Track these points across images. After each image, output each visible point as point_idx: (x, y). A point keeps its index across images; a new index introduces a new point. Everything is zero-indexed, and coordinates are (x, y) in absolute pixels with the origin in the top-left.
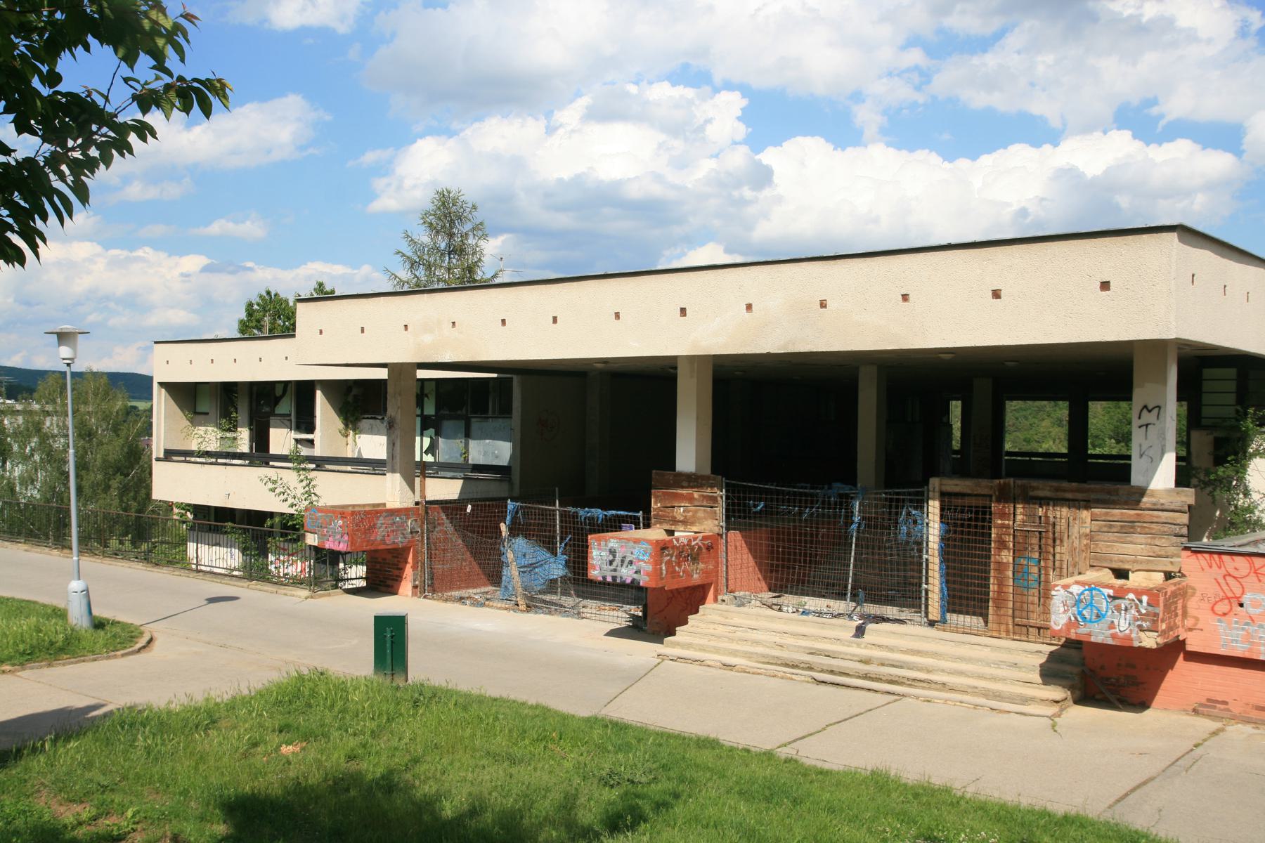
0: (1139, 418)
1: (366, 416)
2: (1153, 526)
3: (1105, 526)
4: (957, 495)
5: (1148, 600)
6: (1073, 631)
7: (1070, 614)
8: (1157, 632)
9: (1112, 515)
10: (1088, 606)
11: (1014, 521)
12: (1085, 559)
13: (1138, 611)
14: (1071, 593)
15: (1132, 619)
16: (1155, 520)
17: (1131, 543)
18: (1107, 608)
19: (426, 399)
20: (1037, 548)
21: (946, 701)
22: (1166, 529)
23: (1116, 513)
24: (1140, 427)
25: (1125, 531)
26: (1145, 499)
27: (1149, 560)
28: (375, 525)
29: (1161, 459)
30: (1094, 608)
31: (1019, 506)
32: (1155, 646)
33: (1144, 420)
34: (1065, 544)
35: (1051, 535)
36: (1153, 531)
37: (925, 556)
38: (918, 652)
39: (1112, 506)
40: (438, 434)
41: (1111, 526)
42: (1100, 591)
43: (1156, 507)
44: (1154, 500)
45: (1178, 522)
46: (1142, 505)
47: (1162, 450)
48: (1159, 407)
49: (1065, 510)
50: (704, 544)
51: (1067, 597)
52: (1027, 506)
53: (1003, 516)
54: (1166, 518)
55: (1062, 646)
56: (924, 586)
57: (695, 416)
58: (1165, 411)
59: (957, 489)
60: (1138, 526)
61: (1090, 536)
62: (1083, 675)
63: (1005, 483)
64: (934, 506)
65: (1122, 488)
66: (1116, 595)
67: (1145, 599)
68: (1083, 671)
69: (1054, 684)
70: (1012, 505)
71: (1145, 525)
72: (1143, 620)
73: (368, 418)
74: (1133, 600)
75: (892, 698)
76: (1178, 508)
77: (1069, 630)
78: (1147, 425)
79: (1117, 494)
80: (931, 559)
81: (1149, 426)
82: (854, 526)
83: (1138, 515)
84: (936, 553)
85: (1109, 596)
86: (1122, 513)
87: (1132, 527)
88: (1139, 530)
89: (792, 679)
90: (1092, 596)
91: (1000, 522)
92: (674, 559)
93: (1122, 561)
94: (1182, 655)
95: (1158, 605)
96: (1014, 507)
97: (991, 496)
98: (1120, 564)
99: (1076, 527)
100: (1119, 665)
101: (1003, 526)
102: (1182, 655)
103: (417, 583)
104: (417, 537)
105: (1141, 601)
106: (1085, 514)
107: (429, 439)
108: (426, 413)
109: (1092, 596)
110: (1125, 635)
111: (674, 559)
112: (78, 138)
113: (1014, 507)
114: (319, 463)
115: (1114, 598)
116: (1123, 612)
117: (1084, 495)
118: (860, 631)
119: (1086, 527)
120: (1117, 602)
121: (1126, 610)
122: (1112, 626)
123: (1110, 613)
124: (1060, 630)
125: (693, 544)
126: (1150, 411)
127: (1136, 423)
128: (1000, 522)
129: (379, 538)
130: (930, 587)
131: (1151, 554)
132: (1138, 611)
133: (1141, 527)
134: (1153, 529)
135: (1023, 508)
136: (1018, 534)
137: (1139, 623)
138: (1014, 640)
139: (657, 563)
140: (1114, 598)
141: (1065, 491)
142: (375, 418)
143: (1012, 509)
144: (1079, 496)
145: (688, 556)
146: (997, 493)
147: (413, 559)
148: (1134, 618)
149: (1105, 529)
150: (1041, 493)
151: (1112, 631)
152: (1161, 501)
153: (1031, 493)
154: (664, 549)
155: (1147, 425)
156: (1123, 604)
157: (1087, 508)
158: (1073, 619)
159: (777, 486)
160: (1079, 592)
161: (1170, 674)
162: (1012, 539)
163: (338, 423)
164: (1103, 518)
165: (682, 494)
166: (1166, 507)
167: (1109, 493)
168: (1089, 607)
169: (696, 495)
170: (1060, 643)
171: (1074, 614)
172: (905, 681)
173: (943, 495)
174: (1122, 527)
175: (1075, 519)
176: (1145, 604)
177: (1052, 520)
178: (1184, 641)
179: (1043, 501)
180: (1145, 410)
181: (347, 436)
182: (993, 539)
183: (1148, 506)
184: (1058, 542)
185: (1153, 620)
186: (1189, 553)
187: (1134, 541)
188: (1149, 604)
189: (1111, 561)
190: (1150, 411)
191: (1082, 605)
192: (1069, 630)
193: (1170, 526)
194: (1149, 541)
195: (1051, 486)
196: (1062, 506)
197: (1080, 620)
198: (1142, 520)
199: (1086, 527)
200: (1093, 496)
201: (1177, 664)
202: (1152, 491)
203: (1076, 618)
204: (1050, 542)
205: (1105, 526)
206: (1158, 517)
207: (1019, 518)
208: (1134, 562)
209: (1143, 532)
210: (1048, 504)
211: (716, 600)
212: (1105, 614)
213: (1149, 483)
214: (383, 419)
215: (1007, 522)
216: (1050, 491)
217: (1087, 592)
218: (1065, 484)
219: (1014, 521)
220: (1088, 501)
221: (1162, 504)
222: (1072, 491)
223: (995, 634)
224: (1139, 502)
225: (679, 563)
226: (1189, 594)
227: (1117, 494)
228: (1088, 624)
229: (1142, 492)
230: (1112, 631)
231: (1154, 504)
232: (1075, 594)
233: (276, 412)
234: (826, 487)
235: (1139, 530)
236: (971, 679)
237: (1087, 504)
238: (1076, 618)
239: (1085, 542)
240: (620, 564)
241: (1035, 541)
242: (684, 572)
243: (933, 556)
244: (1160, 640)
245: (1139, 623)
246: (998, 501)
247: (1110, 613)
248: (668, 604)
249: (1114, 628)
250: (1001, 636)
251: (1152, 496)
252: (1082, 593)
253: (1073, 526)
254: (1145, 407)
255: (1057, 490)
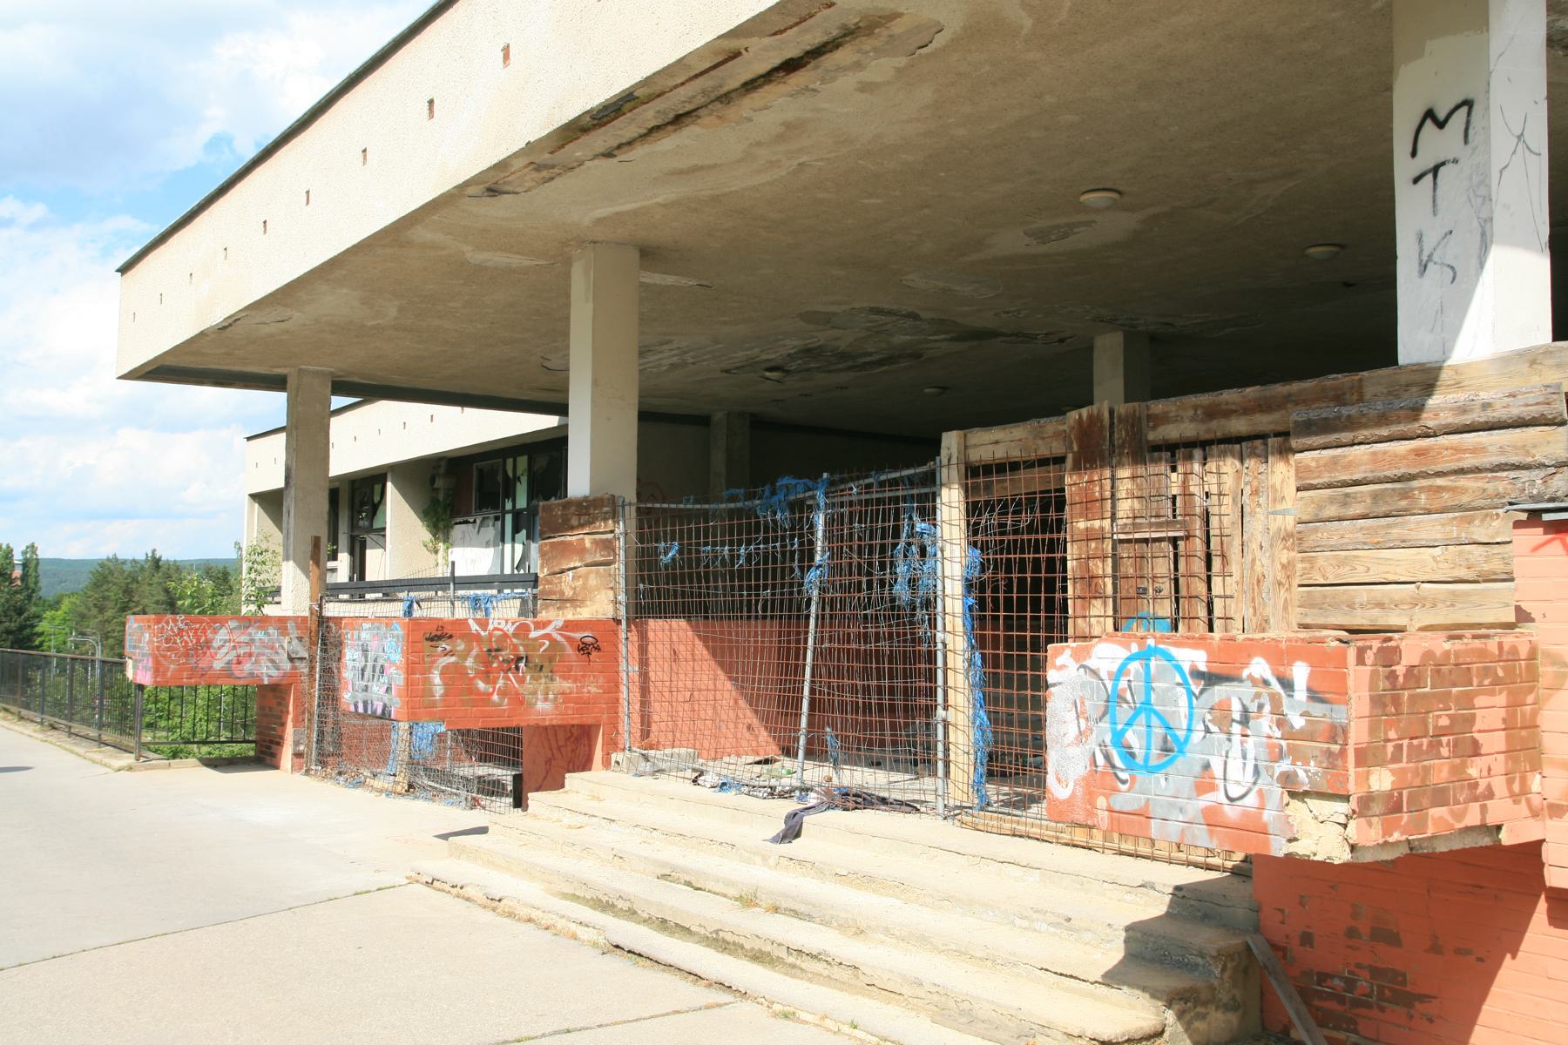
0: (1414, 154)
1: (458, 520)
2: (1462, 481)
3: (1332, 500)
4: (1001, 468)
5: (1312, 676)
6: (1101, 802)
7: (1092, 744)
8: (1346, 798)
9: (1349, 466)
10: (1137, 712)
11: (1113, 518)
12: (1285, 608)
13: (1282, 723)
14: (1095, 673)
15: (1263, 755)
16: (1469, 461)
17: (1405, 545)
18: (1191, 717)
19: (518, 484)
20: (1167, 587)
21: (825, 1017)
22: (1501, 487)
23: (1359, 457)
24: (1416, 180)
25: (1383, 509)
26: (1434, 401)
27: (1453, 593)
28: (208, 643)
29: (1482, 265)
30: (1154, 721)
31: (1124, 473)
32: (1342, 856)
33: (1425, 160)
34: (1234, 568)
35: (1198, 545)
36: (1465, 499)
37: (940, 636)
38: (866, 880)
39: (1346, 436)
40: (530, 537)
41: (1346, 501)
42: (1170, 658)
43: (1467, 419)
44: (1461, 397)
45: (1539, 458)
46: (1428, 420)
47: (1483, 234)
48: (1468, 103)
49: (1230, 465)
50: (569, 639)
51: (1083, 685)
52: (1140, 470)
53: (1089, 506)
54: (1502, 450)
55: (1236, 872)
56: (940, 712)
57: (589, 382)
58: (1487, 108)
59: (1000, 453)
60: (1421, 489)
61: (1295, 539)
62: (1244, 964)
63: (1090, 416)
64: (951, 502)
65: (1374, 380)
66: (1217, 668)
67: (1300, 673)
68: (1248, 948)
69: (1132, 985)
70: (1107, 473)
71: (1440, 482)
72: (1297, 755)
73: (460, 523)
74: (1266, 683)
75: (725, 997)
76: (1534, 411)
77: (1090, 798)
78: (1435, 170)
79: (1361, 399)
80: (949, 639)
81: (1442, 170)
82: (812, 575)
83: (1419, 453)
84: (960, 628)
85: (1197, 674)
86: (1374, 454)
87: (1405, 495)
88: (1423, 499)
89: (574, 937)
90: (1148, 680)
91: (1082, 525)
92: (469, 662)
93: (1380, 605)
94: (1542, 905)
95: (1342, 694)
96: (1113, 479)
97: (1060, 460)
98: (1376, 612)
99: (1260, 514)
100: (1352, 933)
101: (1089, 536)
102: (1542, 905)
103: (302, 748)
104: (303, 668)
105: (1287, 685)
106: (1281, 473)
107: (521, 546)
108: (518, 507)
109: (1148, 680)
110: (1245, 814)
111: (469, 662)
112: (1505, 672)
113: (1113, 479)
114: (388, 590)
115: (1210, 679)
116: (1236, 728)
117: (1276, 416)
118: (792, 831)
119: (1284, 513)
120: (1219, 691)
121: (1245, 721)
122: (1204, 783)
123: (1197, 736)
124: (1070, 801)
125: (533, 634)
126: (1441, 125)
127: (1403, 168)
128: (1082, 525)
129: (218, 665)
130: (951, 715)
131: (1462, 573)
132: (1282, 723)
133: (1430, 489)
134: (1464, 490)
135: (1133, 478)
136: (1124, 552)
137: (1284, 766)
138: (1122, 853)
139: (415, 667)
140: (1210, 679)
141: (1228, 414)
142: (466, 522)
143: (1107, 484)
144: (1264, 422)
145: (519, 659)
146: (1075, 448)
147: (296, 707)
148: (1271, 747)
149: (1331, 511)
150: (1171, 432)
151: (1207, 800)
152: (1484, 396)
153: (1152, 436)
154: (435, 638)
155: (1435, 170)
156: (1234, 696)
157: (1285, 451)
158: (1100, 760)
159: (697, 502)
160: (1115, 667)
161: (1509, 973)
162: (1109, 570)
163: (423, 533)
164: (1325, 479)
165: (570, 543)
166: (1498, 414)
167: (1339, 399)
168: (1142, 718)
169: (588, 541)
170: (1229, 864)
171: (1102, 745)
172: (783, 953)
173: (974, 473)
174: (1376, 497)
175: (1255, 492)
176: (1301, 694)
177: (1199, 502)
178: (1532, 852)
179: (1175, 451)
180: (1429, 122)
181: (436, 552)
182: (1070, 574)
183: (1447, 418)
184: (1217, 563)
185: (1329, 753)
186: (1536, 535)
187: (1414, 535)
188: (1314, 695)
189: (1351, 606)
190: (1441, 125)
191: (1124, 712)
192: (1090, 798)
193: (1512, 474)
194: (1454, 531)
195: (1195, 408)
196: (1222, 455)
197: (1118, 762)
198: (1433, 468)
199: (1284, 513)
200: (1296, 415)
201: (1528, 936)
202: (1456, 369)
203: (1107, 757)
204: (1198, 566)
205: (1332, 500)
206: (1477, 450)
207: (1125, 507)
208: (1414, 603)
209: (1436, 505)
210: (1189, 458)
211: (607, 764)
212: (1187, 739)
213: (1446, 352)
214: (475, 522)
215: (1097, 524)
216: (1192, 420)
217: (1135, 666)
218: (1229, 396)
219: (1113, 518)
220: (1286, 434)
221: (1486, 406)
222: (1246, 410)
223: (1080, 836)
224: (1416, 411)
225: (487, 673)
226: (1543, 682)
227: (1361, 399)
228: (1141, 776)
229: (1428, 379)
230: (1207, 800)
231: (1463, 410)
232: (1104, 675)
233: (375, 527)
234: (767, 489)
235: (1423, 499)
236: (643, 930)
237: (1278, 442)
238: (1107, 757)
239: (1284, 556)
240: (276, 658)
241: (1163, 567)
242: (502, 693)
243: (953, 633)
244: (1368, 833)
245: (1284, 766)
246: (1077, 467)
247: (1197, 736)
248: (547, 773)
249: (1212, 788)
250: (1092, 843)
251: (1458, 385)
252: (1122, 671)
253: (1253, 513)
254: (1430, 114)
255: (1212, 413)
